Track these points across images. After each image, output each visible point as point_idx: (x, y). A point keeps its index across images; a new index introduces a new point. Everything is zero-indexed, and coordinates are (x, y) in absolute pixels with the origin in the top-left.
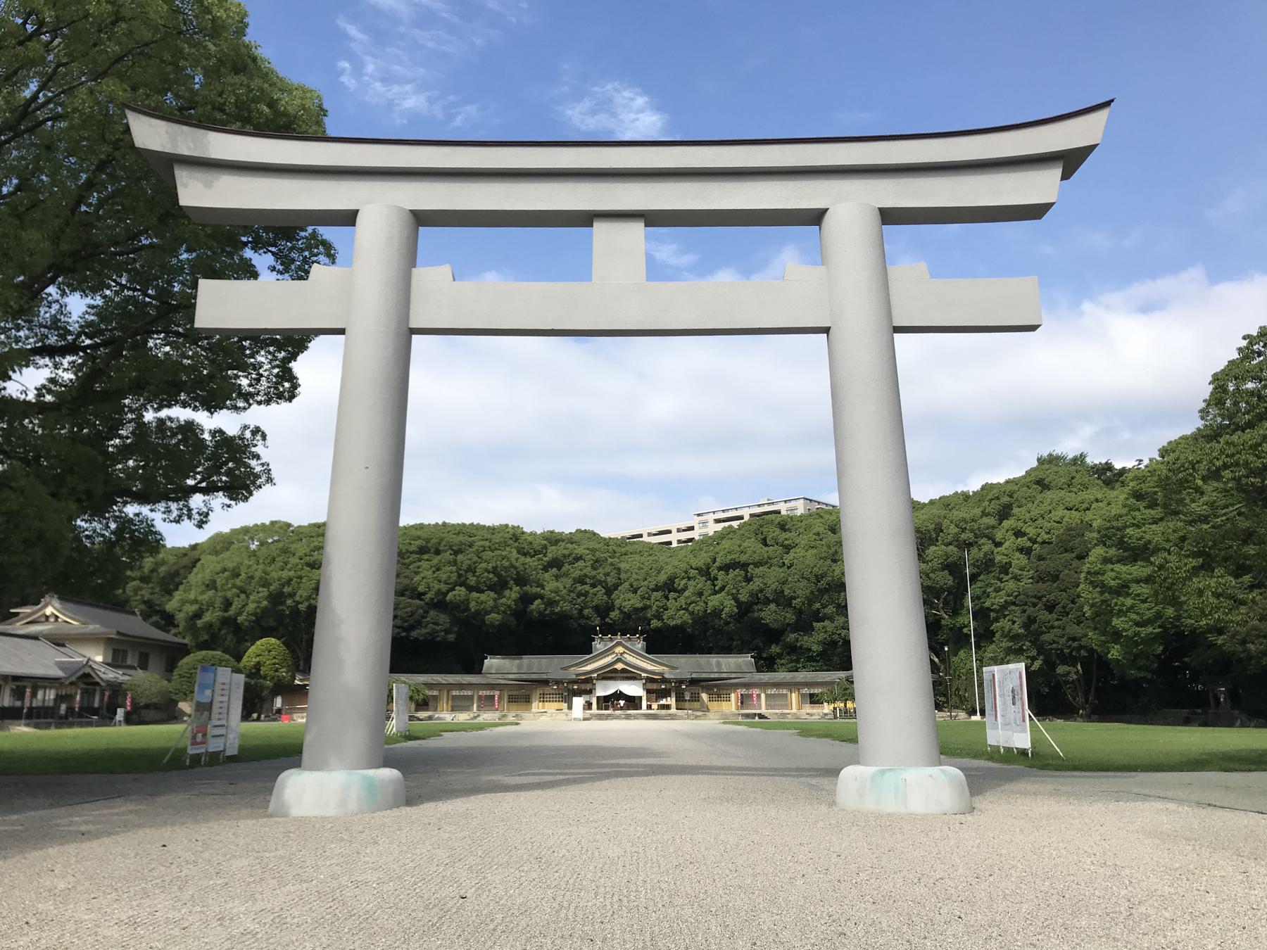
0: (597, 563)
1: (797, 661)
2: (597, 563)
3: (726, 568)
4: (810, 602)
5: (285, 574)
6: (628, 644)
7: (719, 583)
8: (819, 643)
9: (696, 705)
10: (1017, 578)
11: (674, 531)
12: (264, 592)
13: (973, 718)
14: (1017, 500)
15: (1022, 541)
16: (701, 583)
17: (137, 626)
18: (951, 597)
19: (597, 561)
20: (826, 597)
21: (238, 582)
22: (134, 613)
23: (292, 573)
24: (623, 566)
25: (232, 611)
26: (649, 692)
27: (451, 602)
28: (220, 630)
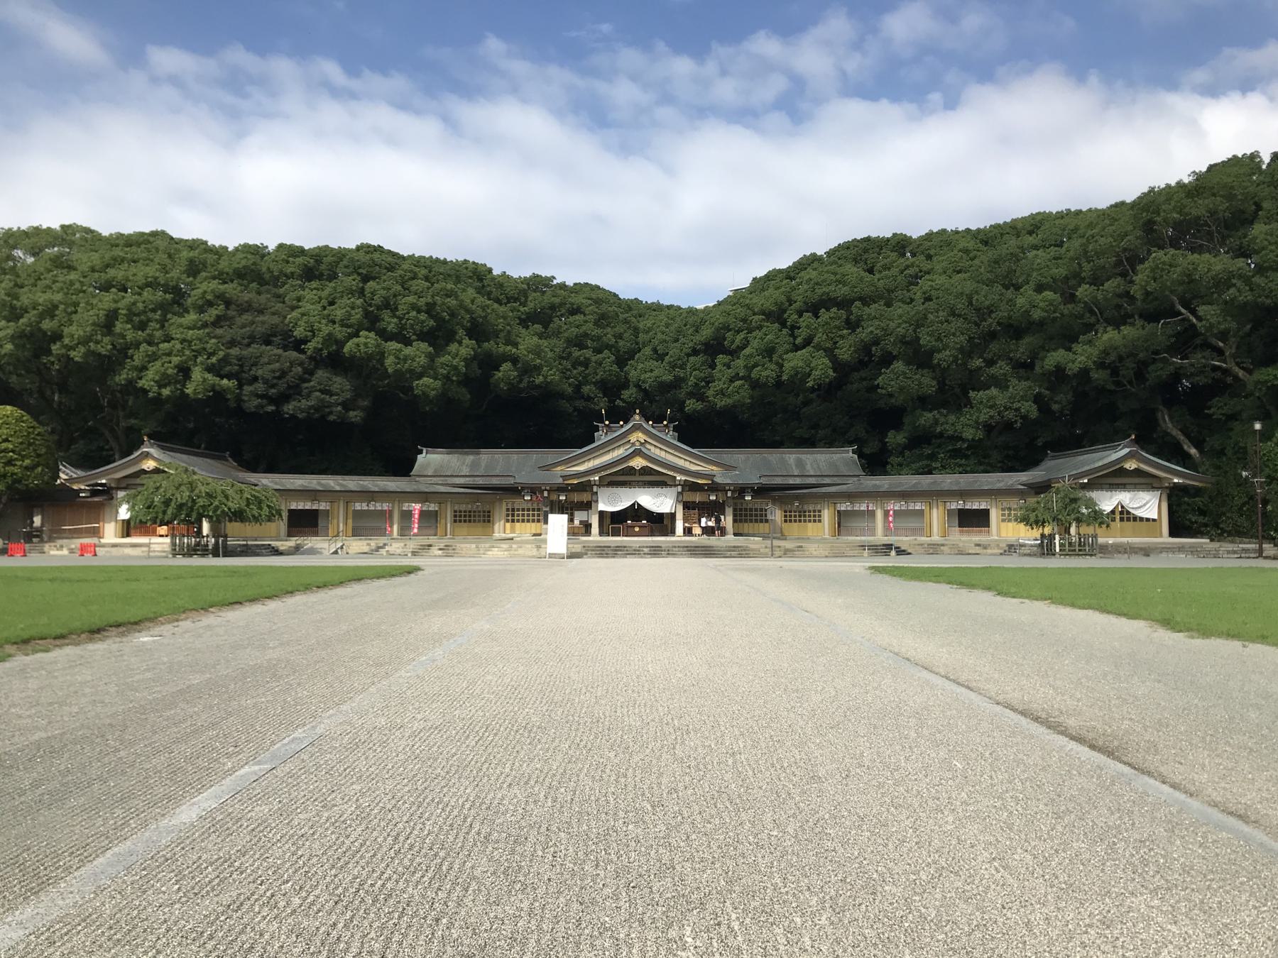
1: (932, 457)
3: (813, 309)
16: (771, 333)
23: (58, 297)
26: (687, 506)
27: (353, 357)
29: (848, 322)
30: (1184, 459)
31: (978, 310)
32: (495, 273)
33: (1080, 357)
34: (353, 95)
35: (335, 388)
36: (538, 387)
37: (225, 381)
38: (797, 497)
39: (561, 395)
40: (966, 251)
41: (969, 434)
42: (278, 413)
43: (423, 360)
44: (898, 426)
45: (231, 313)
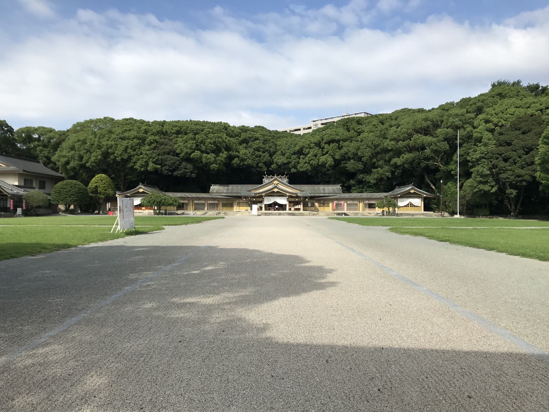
0: (265, 141)
1: (363, 188)
2: (265, 141)
3: (329, 143)
4: (371, 158)
5: (110, 143)
6: (280, 180)
7: (325, 150)
8: (374, 179)
9: (313, 208)
10: (486, 145)
12: (99, 152)
13: (456, 216)
14: (487, 104)
15: (491, 126)
16: (316, 150)
17: (39, 168)
18: (445, 156)
19: (265, 140)
20: (379, 156)
21: (86, 147)
22: (39, 162)
24: (277, 143)
25: (84, 161)
26: (290, 202)
27: (193, 158)
28: (79, 170)
29: (339, 146)
31: (375, 145)
33: (398, 161)
34: (161, 29)
35: (188, 167)
36: (245, 165)
37: (158, 166)
39: (252, 167)
40: (374, 125)
41: (372, 181)
42: (172, 175)
43: (213, 159)
44: (353, 179)
45: (158, 145)
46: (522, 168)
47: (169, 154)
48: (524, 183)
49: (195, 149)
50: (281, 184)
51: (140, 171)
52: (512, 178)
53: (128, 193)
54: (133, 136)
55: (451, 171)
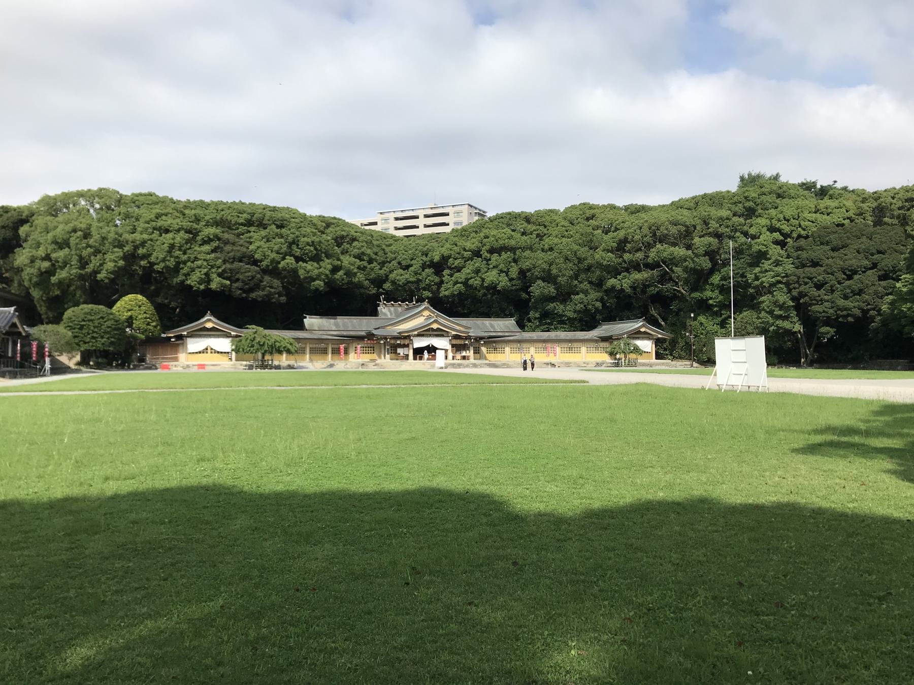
3: (492, 251)
11: (421, 217)
12: (119, 252)
26: (453, 346)
30: (659, 326)
32: (758, 344)
35: (275, 285)
38: (494, 342)
41: (571, 315)
46: (846, 297)
47: (241, 261)
48: (850, 319)
49: (286, 254)
50: (423, 316)
51: (198, 291)
52: (831, 311)
53: (184, 330)
54: (176, 227)
55: (707, 300)
